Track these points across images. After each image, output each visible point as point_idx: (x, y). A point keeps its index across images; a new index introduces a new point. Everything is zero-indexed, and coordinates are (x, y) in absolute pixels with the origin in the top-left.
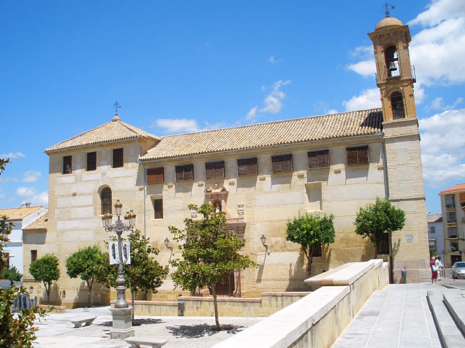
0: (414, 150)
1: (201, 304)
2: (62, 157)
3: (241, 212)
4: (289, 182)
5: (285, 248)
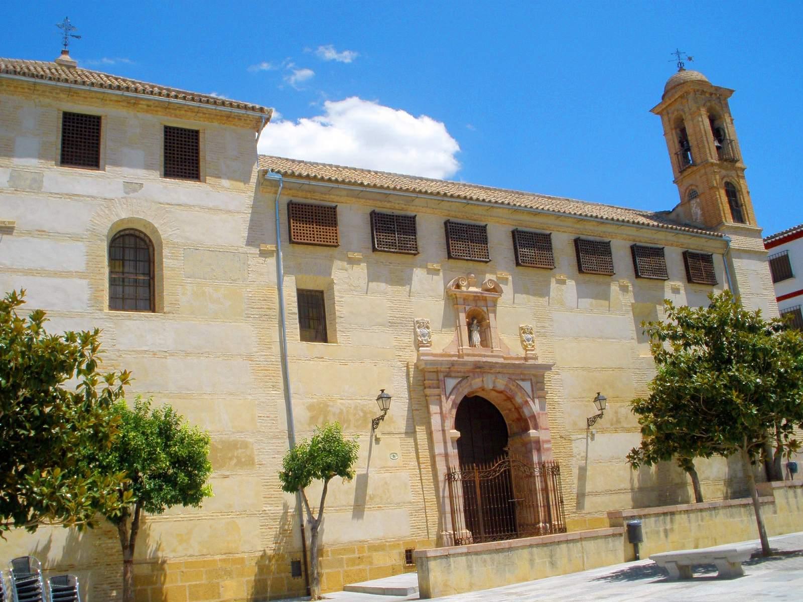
1: (672, 521)
4: (606, 296)
5: (619, 426)
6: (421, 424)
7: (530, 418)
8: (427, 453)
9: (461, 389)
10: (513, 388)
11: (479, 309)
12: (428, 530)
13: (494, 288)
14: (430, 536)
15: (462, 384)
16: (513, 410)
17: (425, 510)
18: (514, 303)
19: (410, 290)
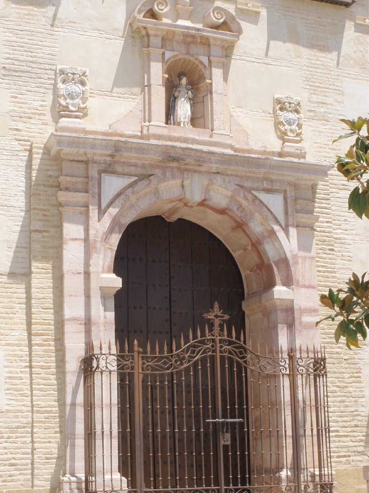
3: (292, 131)
6: (44, 258)
7: (276, 263)
8: (50, 316)
9: (133, 199)
10: (245, 203)
11: (192, 59)
12: (33, 469)
13: (225, 23)
14: (36, 482)
15: (136, 188)
16: (249, 248)
17: (32, 427)
18: (267, 55)
19: (55, 15)
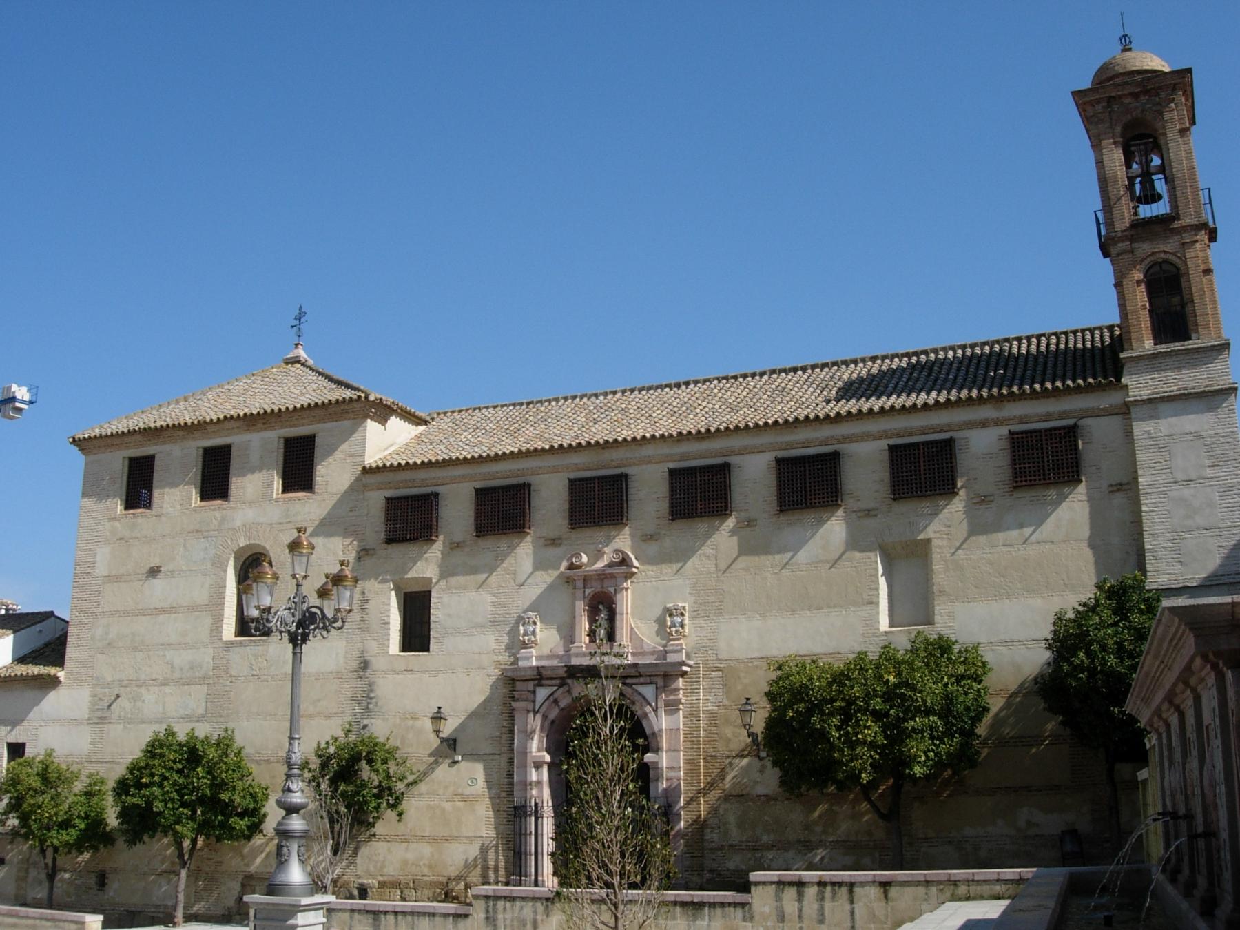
0: (1223, 437)
2: (124, 458)
